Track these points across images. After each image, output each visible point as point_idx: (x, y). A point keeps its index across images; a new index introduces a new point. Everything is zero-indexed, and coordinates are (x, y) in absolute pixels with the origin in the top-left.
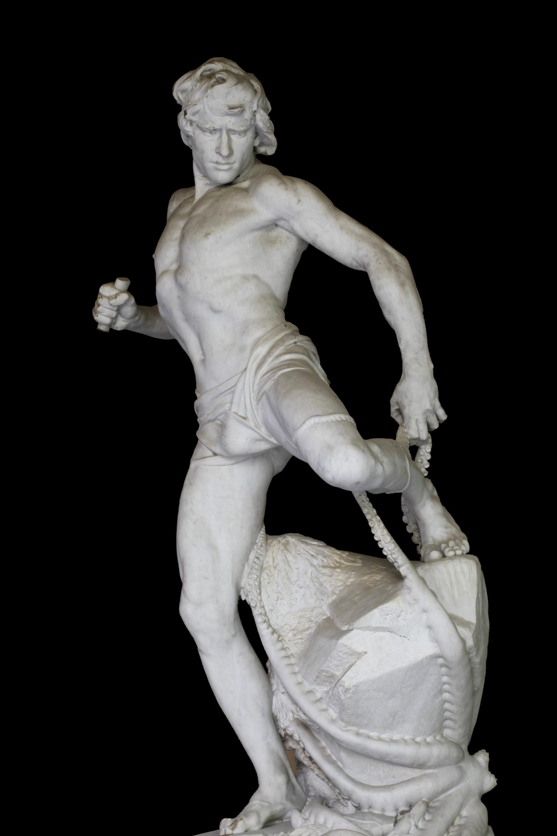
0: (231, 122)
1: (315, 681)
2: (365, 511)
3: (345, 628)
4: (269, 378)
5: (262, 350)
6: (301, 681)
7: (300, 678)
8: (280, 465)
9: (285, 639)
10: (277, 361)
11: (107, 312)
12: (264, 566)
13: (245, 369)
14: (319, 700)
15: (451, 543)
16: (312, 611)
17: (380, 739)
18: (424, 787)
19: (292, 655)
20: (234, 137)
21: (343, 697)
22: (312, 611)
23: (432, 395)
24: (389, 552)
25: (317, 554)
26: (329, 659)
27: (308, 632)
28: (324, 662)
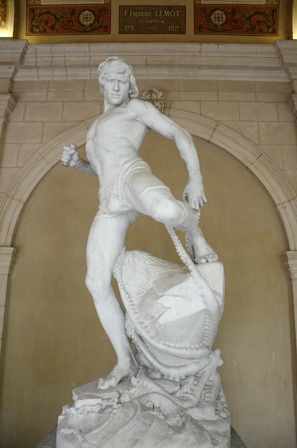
0: (119, 77)
1: (145, 318)
2: (173, 237)
3: (160, 294)
4: (129, 176)
5: (127, 166)
6: (138, 317)
7: (137, 316)
8: (133, 218)
9: (132, 297)
10: (133, 169)
11: (66, 157)
12: (124, 263)
13: (119, 175)
14: (146, 327)
15: (210, 256)
16: (145, 284)
17: (175, 347)
18: (192, 368)
19: (135, 304)
20: (121, 84)
21: (158, 329)
22: (145, 284)
23: (202, 190)
24: (184, 258)
25: (148, 259)
26: (152, 309)
27: (142, 294)
28: (149, 310)
